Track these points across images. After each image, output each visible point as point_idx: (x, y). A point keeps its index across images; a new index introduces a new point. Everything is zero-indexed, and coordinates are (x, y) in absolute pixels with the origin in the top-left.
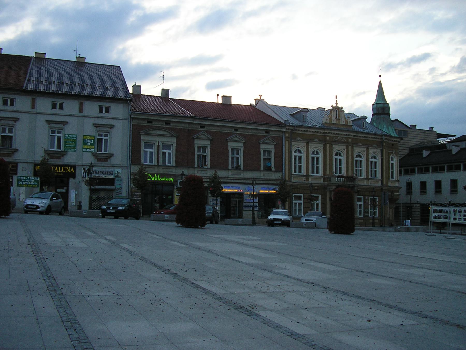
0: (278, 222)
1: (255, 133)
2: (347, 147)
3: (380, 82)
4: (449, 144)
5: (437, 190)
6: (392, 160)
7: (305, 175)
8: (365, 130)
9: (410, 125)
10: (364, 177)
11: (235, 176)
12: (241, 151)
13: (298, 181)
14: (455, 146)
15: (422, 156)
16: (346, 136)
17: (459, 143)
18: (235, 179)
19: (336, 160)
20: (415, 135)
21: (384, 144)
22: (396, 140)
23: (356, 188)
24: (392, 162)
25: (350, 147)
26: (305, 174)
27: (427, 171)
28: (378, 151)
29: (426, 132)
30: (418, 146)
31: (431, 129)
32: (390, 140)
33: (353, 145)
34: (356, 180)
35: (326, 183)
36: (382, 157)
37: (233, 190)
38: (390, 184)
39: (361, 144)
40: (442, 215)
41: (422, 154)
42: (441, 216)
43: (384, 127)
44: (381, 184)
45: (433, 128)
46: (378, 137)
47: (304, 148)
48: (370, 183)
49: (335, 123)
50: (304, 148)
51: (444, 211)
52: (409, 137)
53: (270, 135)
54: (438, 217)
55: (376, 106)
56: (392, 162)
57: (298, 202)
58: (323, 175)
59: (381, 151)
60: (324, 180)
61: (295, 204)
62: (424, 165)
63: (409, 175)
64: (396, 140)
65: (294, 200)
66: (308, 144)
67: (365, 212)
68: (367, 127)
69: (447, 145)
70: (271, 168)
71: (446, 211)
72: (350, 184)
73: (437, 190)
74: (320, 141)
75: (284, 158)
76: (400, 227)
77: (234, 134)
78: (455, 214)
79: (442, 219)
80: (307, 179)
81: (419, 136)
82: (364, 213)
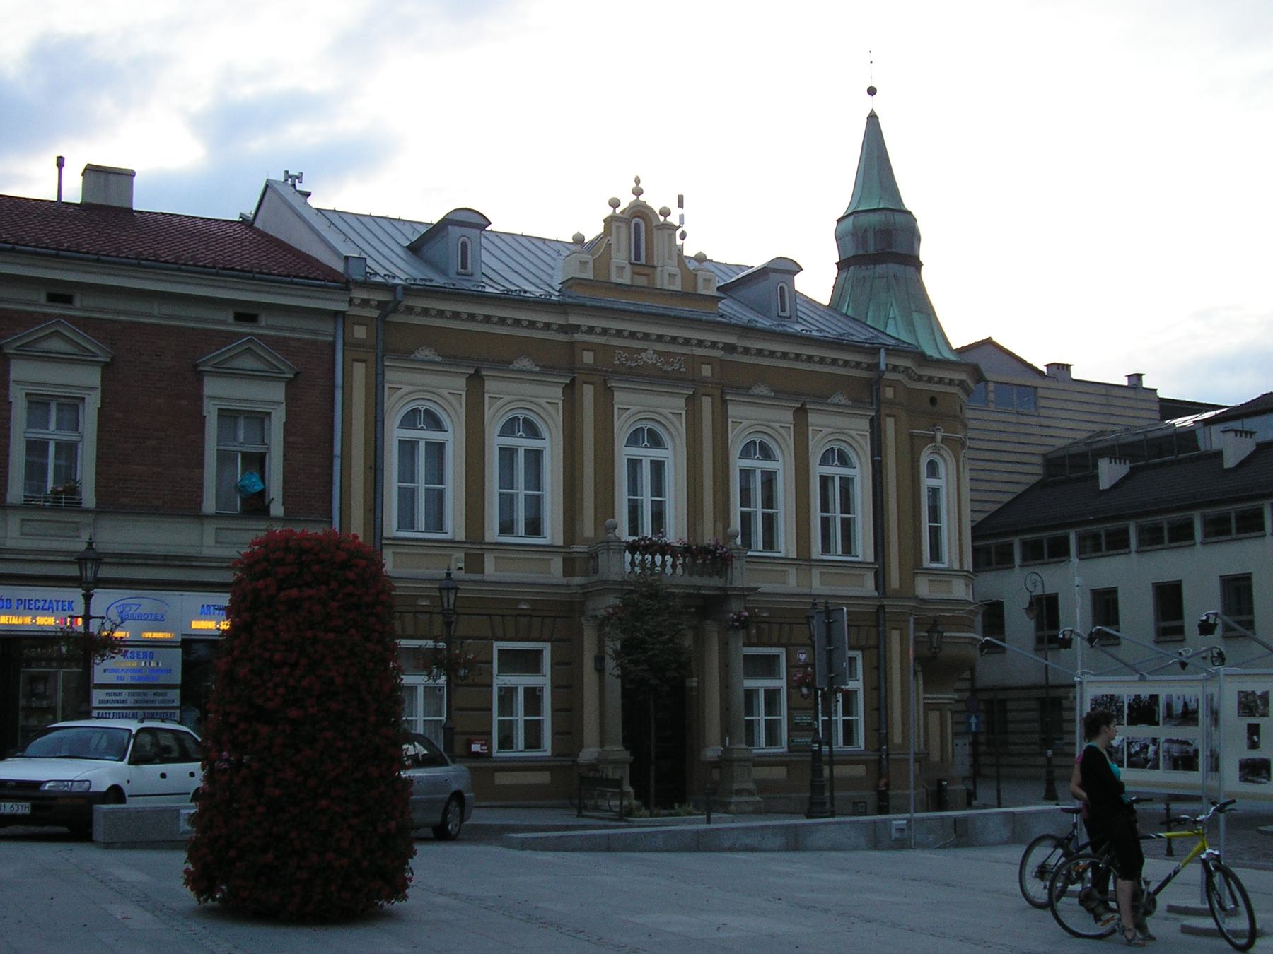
0: (9, 805)
1: (170, 317)
2: (692, 401)
3: (873, 119)
4: (1207, 428)
5: (1167, 624)
6: (933, 470)
7: (457, 539)
8: (788, 324)
9: (1048, 366)
10: (787, 550)
11: (44, 544)
12: (86, 408)
13: (420, 571)
14: (1236, 431)
15: (1098, 482)
16: (686, 350)
17: (1249, 424)
18: (40, 556)
19: (634, 464)
20: (1070, 406)
21: (889, 393)
22: (948, 375)
23: (736, 607)
24: (933, 482)
25: (706, 403)
26: (461, 536)
27: (1118, 543)
28: (857, 428)
29: (1114, 392)
30: (1083, 448)
31: (1134, 381)
32: (920, 378)
33: (722, 393)
34: (736, 563)
35: (578, 580)
36: (880, 454)
37: (28, 620)
38: (923, 588)
39: (766, 392)
40: (1154, 741)
41: (1096, 477)
42: (1146, 747)
43: (891, 315)
44: (877, 589)
45: (1141, 375)
46: (853, 357)
47: (457, 406)
48: (818, 584)
49: (626, 280)
50: (457, 406)
51: (1169, 707)
52: (1043, 412)
53: (261, 332)
54: (1130, 755)
55: (854, 227)
56: (933, 482)
57: (521, 681)
58: (561, 543)
59: (872, 426)
60: (570, 566)
61: (507, 695)
62: (1106, 519)
63: (1043, 564)
64: (948, 375)
65: (501, 672)
66: (476, 381)
67: (793, 727)
68: (799, 314)
69: (1199, 433)
70: (267, 502)
71: (1185, 705)
72: (705, 587)
73: (1167, 624)
74: (547, 369)
75: (337, 449)
76: (909, 821)
77: (47, 317)
78: (1253, 730)
79: (1156, 767)
80: (474, 562)
81: (1087, 417)
82: (789, 731)
